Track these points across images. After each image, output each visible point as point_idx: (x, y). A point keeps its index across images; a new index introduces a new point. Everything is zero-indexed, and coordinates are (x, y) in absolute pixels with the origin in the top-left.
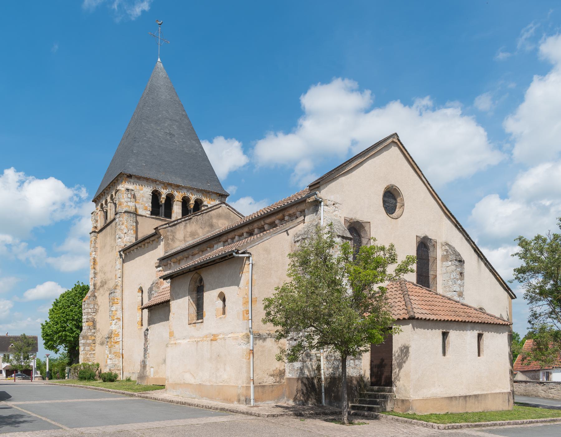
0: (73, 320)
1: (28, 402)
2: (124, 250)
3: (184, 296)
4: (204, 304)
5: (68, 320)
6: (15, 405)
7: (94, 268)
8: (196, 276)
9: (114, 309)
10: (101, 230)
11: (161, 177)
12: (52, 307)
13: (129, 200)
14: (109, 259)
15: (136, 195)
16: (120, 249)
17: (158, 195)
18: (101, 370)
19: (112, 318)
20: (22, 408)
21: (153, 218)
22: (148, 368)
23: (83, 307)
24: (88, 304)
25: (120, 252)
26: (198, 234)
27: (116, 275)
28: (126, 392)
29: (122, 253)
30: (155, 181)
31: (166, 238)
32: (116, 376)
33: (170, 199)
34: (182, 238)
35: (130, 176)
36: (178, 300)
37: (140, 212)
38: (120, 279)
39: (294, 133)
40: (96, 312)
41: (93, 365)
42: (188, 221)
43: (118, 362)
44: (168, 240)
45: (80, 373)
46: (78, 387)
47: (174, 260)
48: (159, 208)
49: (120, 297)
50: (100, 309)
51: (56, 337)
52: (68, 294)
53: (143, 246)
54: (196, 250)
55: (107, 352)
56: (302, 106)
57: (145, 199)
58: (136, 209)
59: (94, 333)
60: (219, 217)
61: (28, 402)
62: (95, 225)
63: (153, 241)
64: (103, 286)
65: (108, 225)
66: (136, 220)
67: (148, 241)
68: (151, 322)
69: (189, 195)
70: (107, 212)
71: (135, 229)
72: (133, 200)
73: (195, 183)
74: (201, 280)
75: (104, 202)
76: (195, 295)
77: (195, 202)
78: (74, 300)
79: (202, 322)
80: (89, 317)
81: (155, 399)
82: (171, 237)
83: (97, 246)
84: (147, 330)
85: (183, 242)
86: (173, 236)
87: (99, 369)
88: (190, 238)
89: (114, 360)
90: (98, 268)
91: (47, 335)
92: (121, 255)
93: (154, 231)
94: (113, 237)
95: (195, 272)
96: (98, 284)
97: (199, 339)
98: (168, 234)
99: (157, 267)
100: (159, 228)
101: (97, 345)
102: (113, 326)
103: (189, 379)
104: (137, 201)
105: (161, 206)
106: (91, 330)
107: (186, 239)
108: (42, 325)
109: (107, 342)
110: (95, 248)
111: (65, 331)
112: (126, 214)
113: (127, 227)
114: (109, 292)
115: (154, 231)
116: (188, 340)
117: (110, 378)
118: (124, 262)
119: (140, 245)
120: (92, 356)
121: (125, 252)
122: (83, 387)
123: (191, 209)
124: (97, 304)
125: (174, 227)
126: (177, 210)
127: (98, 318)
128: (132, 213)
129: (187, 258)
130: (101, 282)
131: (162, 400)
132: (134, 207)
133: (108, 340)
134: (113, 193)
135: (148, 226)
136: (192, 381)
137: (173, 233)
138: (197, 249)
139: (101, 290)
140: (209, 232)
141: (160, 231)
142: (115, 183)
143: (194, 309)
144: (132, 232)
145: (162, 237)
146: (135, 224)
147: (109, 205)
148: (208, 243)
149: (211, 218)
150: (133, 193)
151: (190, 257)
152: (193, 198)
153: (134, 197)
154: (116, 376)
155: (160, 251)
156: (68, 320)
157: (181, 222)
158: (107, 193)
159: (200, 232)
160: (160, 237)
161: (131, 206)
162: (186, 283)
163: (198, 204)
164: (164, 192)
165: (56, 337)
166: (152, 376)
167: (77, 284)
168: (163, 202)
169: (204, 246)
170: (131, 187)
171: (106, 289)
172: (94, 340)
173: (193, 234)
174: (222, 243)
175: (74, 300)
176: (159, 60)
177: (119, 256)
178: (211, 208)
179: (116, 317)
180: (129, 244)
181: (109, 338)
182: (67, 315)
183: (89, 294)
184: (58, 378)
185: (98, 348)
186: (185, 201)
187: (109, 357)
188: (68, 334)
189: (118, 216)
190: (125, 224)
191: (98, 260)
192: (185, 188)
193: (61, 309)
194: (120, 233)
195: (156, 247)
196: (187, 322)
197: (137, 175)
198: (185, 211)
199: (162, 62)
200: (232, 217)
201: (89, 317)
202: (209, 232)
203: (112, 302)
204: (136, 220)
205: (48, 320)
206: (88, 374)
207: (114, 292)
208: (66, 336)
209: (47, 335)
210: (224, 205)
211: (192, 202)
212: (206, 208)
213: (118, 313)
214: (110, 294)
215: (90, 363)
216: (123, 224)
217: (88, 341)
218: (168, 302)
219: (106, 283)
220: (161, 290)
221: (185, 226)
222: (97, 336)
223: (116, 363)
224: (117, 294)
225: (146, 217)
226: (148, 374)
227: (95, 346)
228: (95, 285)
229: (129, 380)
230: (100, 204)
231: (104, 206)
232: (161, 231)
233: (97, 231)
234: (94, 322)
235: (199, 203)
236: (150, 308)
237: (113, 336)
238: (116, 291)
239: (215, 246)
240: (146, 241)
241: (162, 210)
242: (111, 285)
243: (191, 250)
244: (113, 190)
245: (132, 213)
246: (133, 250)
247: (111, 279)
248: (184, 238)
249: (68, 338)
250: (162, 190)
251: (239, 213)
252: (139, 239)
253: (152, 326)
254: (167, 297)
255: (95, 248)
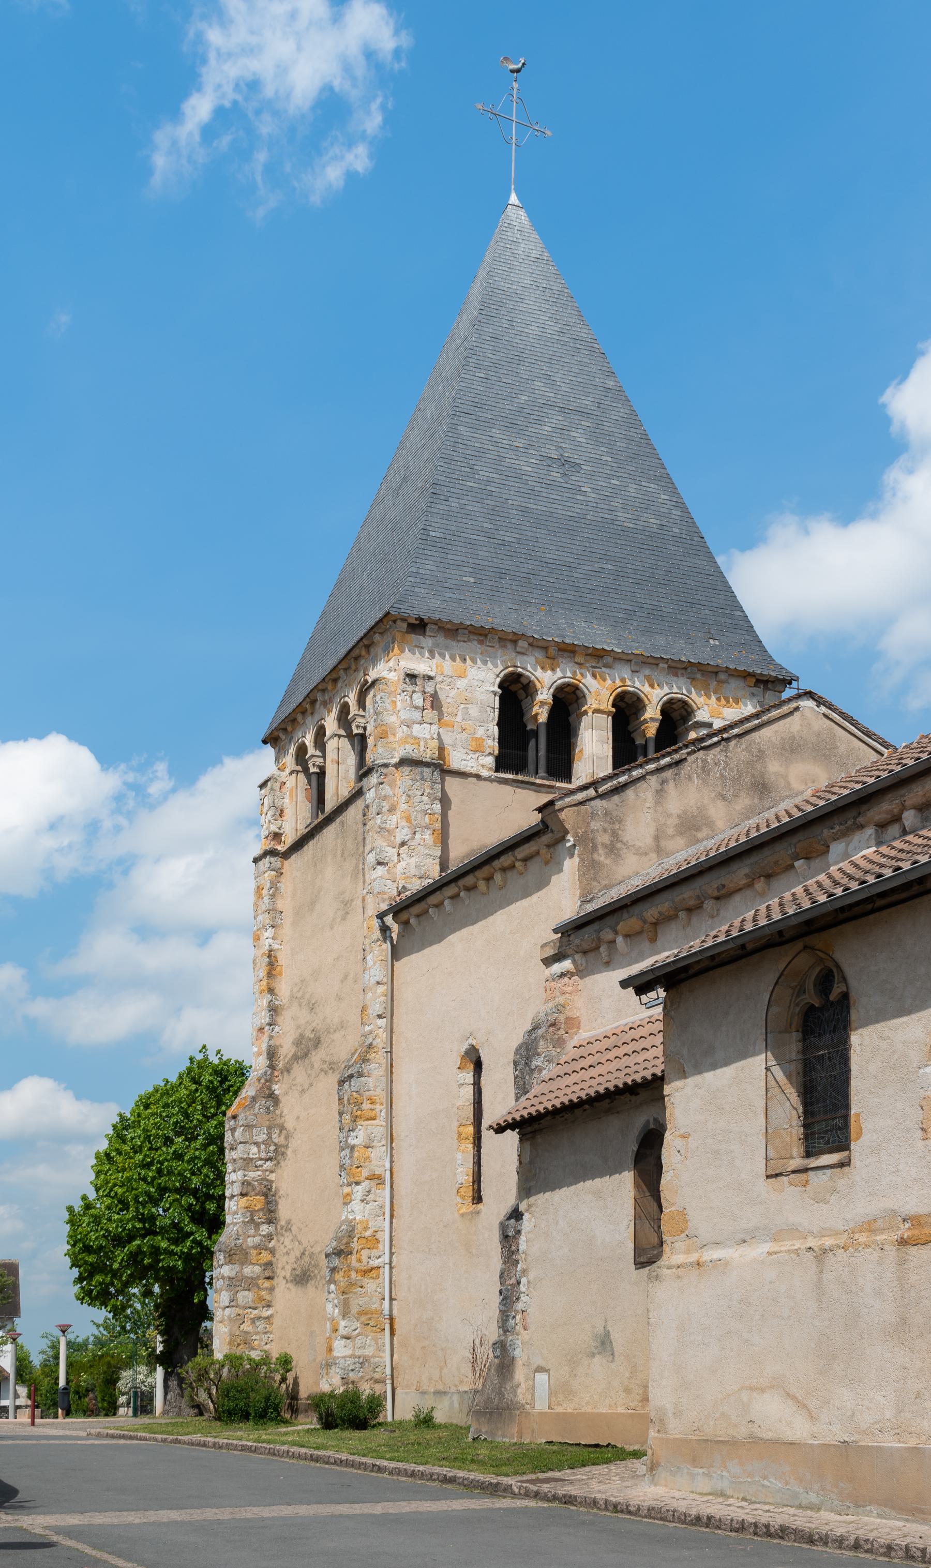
0: (184, 1190)
1: (99, 1519)
2: (400, 910)
3: (744, 1055)
4: (855, 1084)
5: (163, 1190)
6: (69, 1532)
7: (271, 991)
8: (804, 961)
9: (358, 1138)
10: (298, 846)
11: (534, 624)
12: (103, 1146)
13: (417, 715)
14: (337, 946)
15: (442, 696)
16: (384, 907)
17: (522, 694)
18: (296, 1383)
19: (350, 1171)
20: (95, 1547)
21: (505, 782)
22: (520, 1374)
23: (228, 1137)
24: (248, 1127)
25: (381, 916)
26: (710, 824)
27: (364, 1009)
28: (461, 1474)
29: (389, 920)
30: (510, 640)
31: (587, 842)
32: (376, 1404)
33: (567, 702)
34: (649, 841)
35: (419, 626)
36: (709, 1076)
37: (457, 759)
38: (382, 1022)
39: (874, 516)
40: (277, 1155)
41: (266, 1361)
42: (668, 774)
43: (374, 1346)
44: (595, 848)
45: (226, 1394)
46: (235, 1448)
47: (629, 923)
48: (525, 749)
49: (380, 1093)
50: (294, 1143)
51: (121, 1255)
52: (166, 1093)
53: (482, 885)
54: (740, 873)
55: (333, 1310)
56: (894, 429)
57: (474, 711)
58: (441, 749)
59: (270, 1237)
60: (792, 751)
61: (99, 1519)
62: (274, 828)
63: (526, 860)
64: (306, 1055)
65: (329, 820)
66: (443, 790)
67: (505, 860)
68: (532, 1181)
69: (638, 684)
70: (322, 774)
71: (438, 825)
72: (430, 714)
73: (661, 640)
74: (828, 977)
75: (309, 740)
76: (794, 1047)
77: (663, 712)
78: (187, 1116)
79: (842, 1165)
80: (253, 1175)
81: (616, 1508)
82: (605, 838)
83: (280, 905)
84: (516, 1215)
85: (654, 856)
86: (615, 834)
87: (290, 1377)
88: (680, 841)
89: (359, 1341)
90: (284, 988)
91: (87, 1249)
92: (385, 929)
93: (536, 818)
94: (349, 866)
95: (799, 945)
96: (287, 1049)
97: (828, 1242)
98: (595, 825)
99: (548, 962)
100: (559, 805)
101: (280, 1283)
102: (356, 1205)
103: (776, 1416)
104: (446, 718)
105: (535, 733)
106: (257, 1226)
107: (663, 843)
108: (70, 1209)
109: (333, 1270)
110: (274, 911)
111: (155, 1233)
112: (406, 770)
113: (408, 820)
114: (334, 1079)
115: (536, 818)
116: (767, 1247)
117: (350, 1414)
118: (396, 954)
119: (469, 880)
120: (261, 1325)
121: (404, 916)
122: (256, 1450)
123: (650, 741)
124: (282, 1128)
125: (616, 798)
126: (594, 746)
127: (285, 1180)
128: (427, 765)
129: (689, 910)
130: (298, 1043)
131: (654, 1513)
132: (435, 744)
133: (336, 1262)
134: (352, 699)
135: (500, 811)
136: (798, 1429)
137: (614, 820)
138: (746, 870)
139: (299, 1073)
140: (752, 811)
141: (562, 816)
142: (356, 659)
143: (789, 1110)
144: (428, 836)
145: (571, 840)
146: (437, 807)
147: (331, 745)
148: (800, 836)
149: (761, 755)
150: (430, 689)
151: (709, 905)
152: (655, 696)
153: (435, 702)
154: (376, 1404)
155: (562, 895)
156: (163, 1190)
157: (642, 778)
158: (325, 704)
159: (718, 813)
160: (563, 839)
161: (422, 737)
162: (756, 994)
163: (676, 717)
164: (546, 681)
165: (121, 1255)
166: (541, 1405)
167: (200, 1057)
168: (543, 718)
169: (782, 851)
170: (421, 666)
171: (317, 1065)
172: (269, 1264)
173: (690, 825)
174: (870, 831)
175: (187, 1116)
176: (514, 199)
177: (377, 934)
178: (724, 729)
179: (365, 1173)
180: (416, 886)
181: (339, 1253)
182: (159, 1172)
183: (249, 1090)
184: (89, 1412)
185: (285, 1296)
186: (626, 710)
187: (342, 1331)
188: (164, 1245)
189: (373, 779)
190: (404, 807)
191: (283, 959)
192: (625, 659)
193: (136, 1150)
194: (380, 842)
195: (542, 883)
196: (760, 1167)
197: (444, 618)
198: (626, 749)
199: (524, 205)
200: (842, 749)
201: (253, 1175)
202: (752, 811)
203: (352, 1111)
204: (443, 790)
205: (92, 1195)
206: (257, 1399)
207: (360, 1075)
208: (156, 1251)
209: (87, 1249)
210: (810, 703)
211: (652, 713)
212: (704, 732)
213: (374, 1154)
214: (341, 1083)
215: (255, 1355)
216: (392, 810)
217: (248, 1270)
218: (649, 1090)
219: (317, 1043)
220: (570, 1052)
221: (660, 793)
222: (281, 1250)
223: (368, 1352)
224: (371, 1082)
225: (478, 777)
226: (522, 1395)
227: (271, 1289)
228: (272, 1054)
229: (425, 1421)
230: (292, 750)
231: (311, 750)
232: (568, 817)
233: (281, 848)
234: (269, 1194)
235: (676, 716)
236: (529, 1127)
237: (355, 1245)
238: (366, 1068)
239: (836, 848)
240: (497, 864)
241: (539, 749)
242: (342, 1047)
243: (714, 874)
244: (350, 685)
245: (427, 765)
246: (438, 906)
247: (342, 1026)
248: (657, 838)
249: (166, 1262)
250: (539, 673)
251: (868, 734)
252: (453, 867)
253: (541, 1199)
254: (649, 1062)
255: (274, 911)
